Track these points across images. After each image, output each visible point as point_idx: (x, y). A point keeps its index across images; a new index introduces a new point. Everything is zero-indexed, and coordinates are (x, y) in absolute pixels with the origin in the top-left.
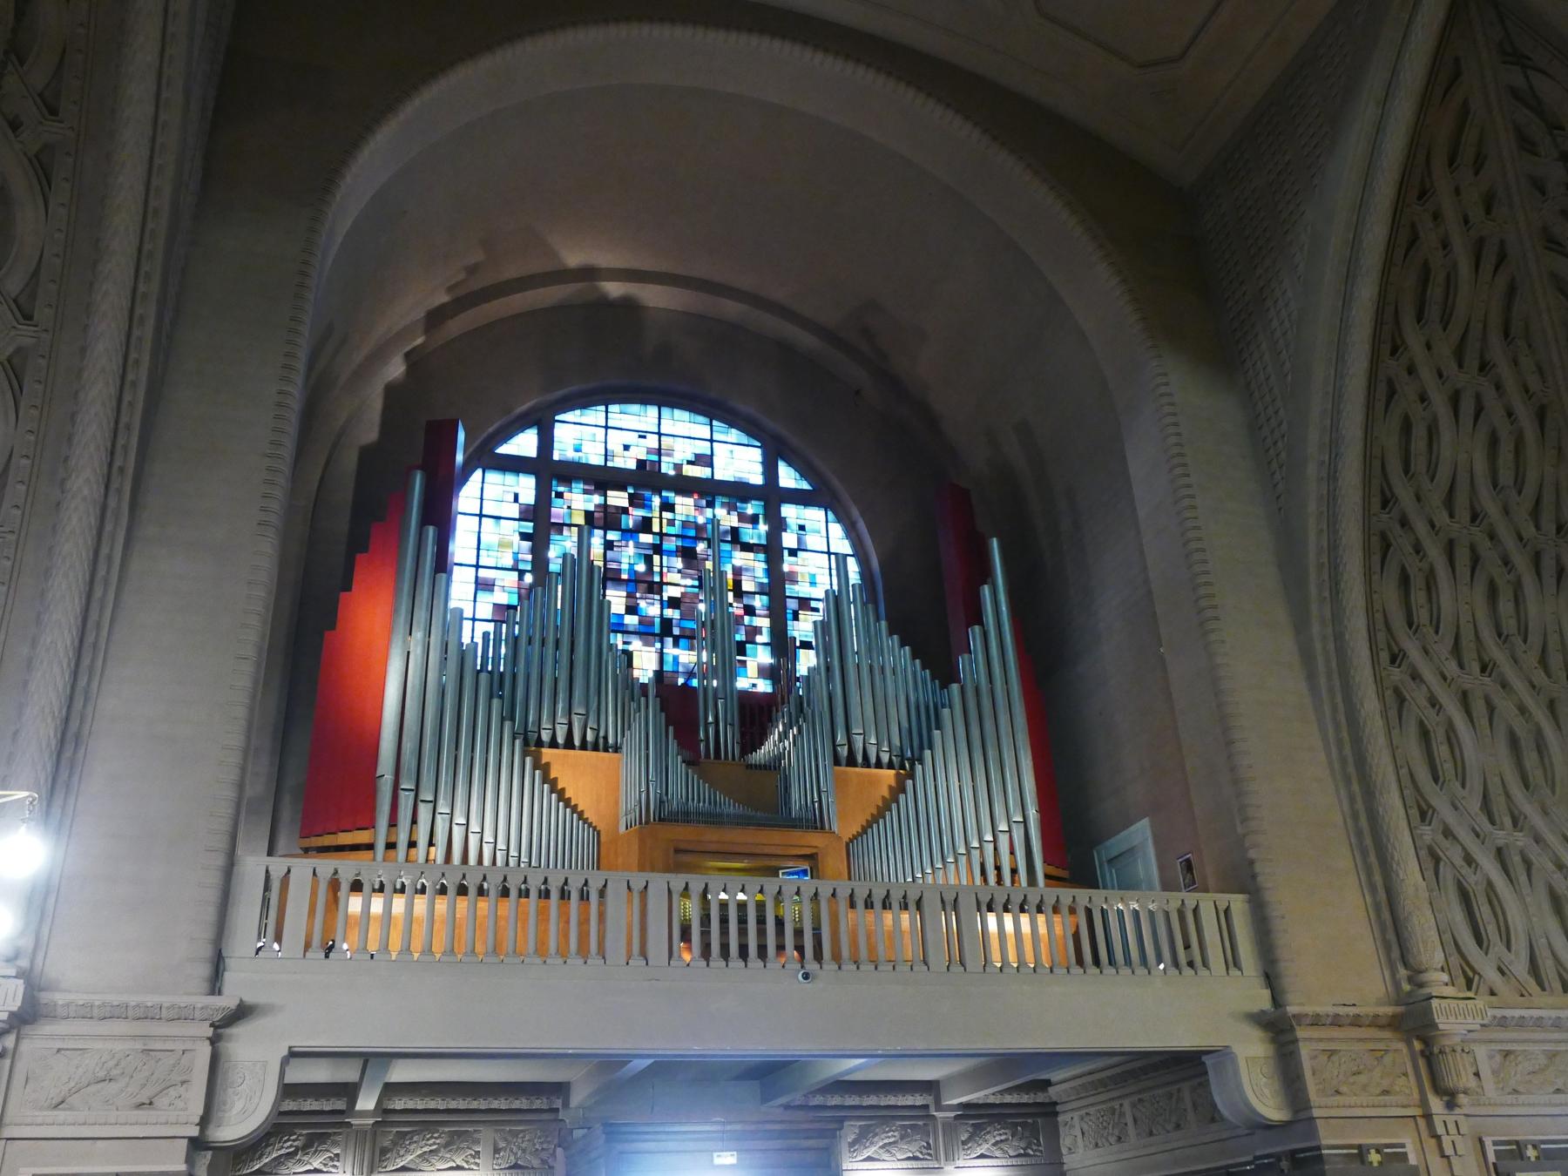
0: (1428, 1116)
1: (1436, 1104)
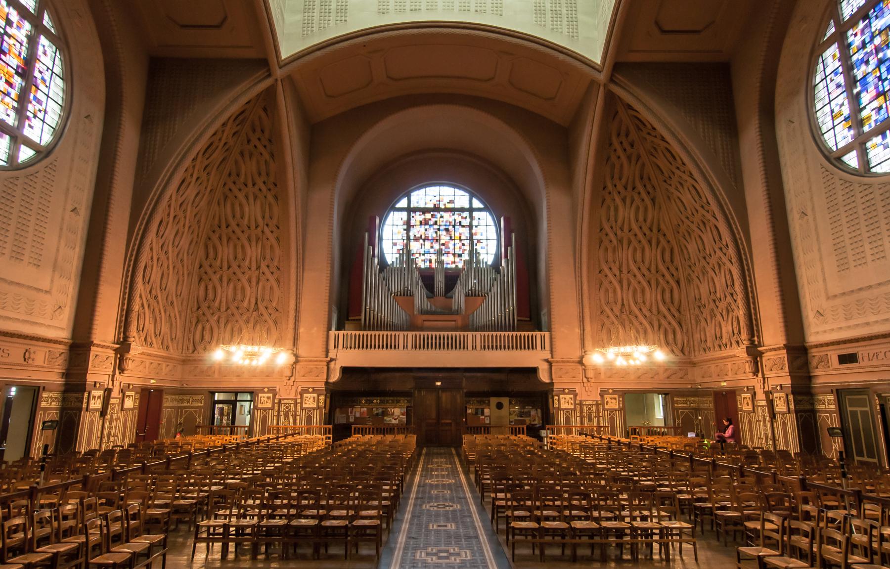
0: (113, 376)
1: (117, 372)
